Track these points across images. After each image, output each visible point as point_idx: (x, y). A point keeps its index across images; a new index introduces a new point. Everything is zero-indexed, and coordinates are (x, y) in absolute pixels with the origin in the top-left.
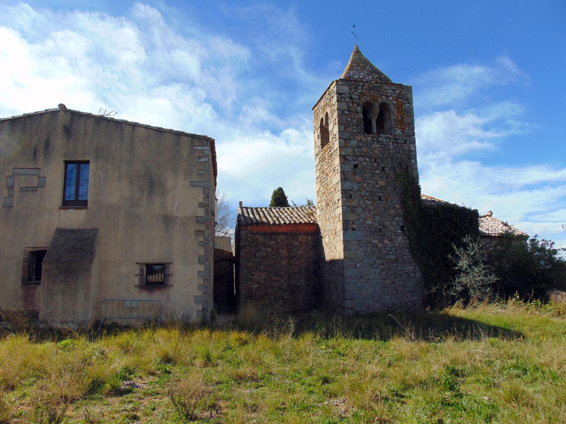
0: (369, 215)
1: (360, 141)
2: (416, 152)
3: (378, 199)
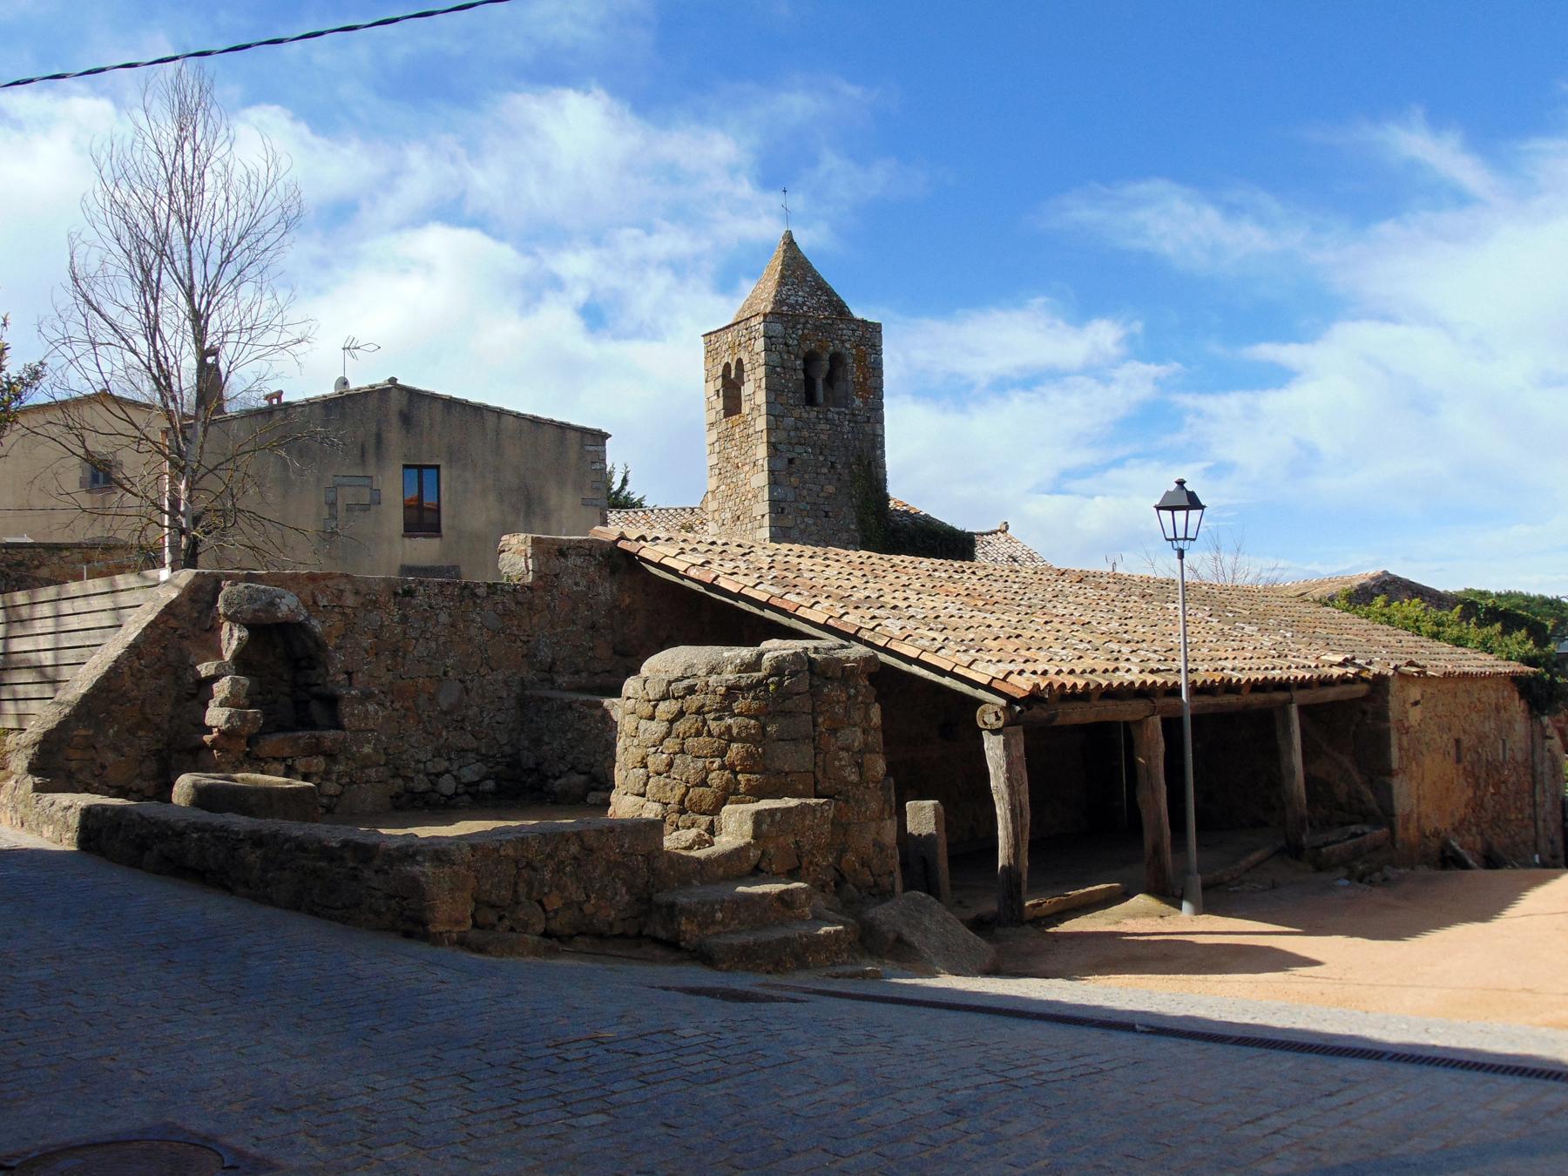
1: (799, 419)
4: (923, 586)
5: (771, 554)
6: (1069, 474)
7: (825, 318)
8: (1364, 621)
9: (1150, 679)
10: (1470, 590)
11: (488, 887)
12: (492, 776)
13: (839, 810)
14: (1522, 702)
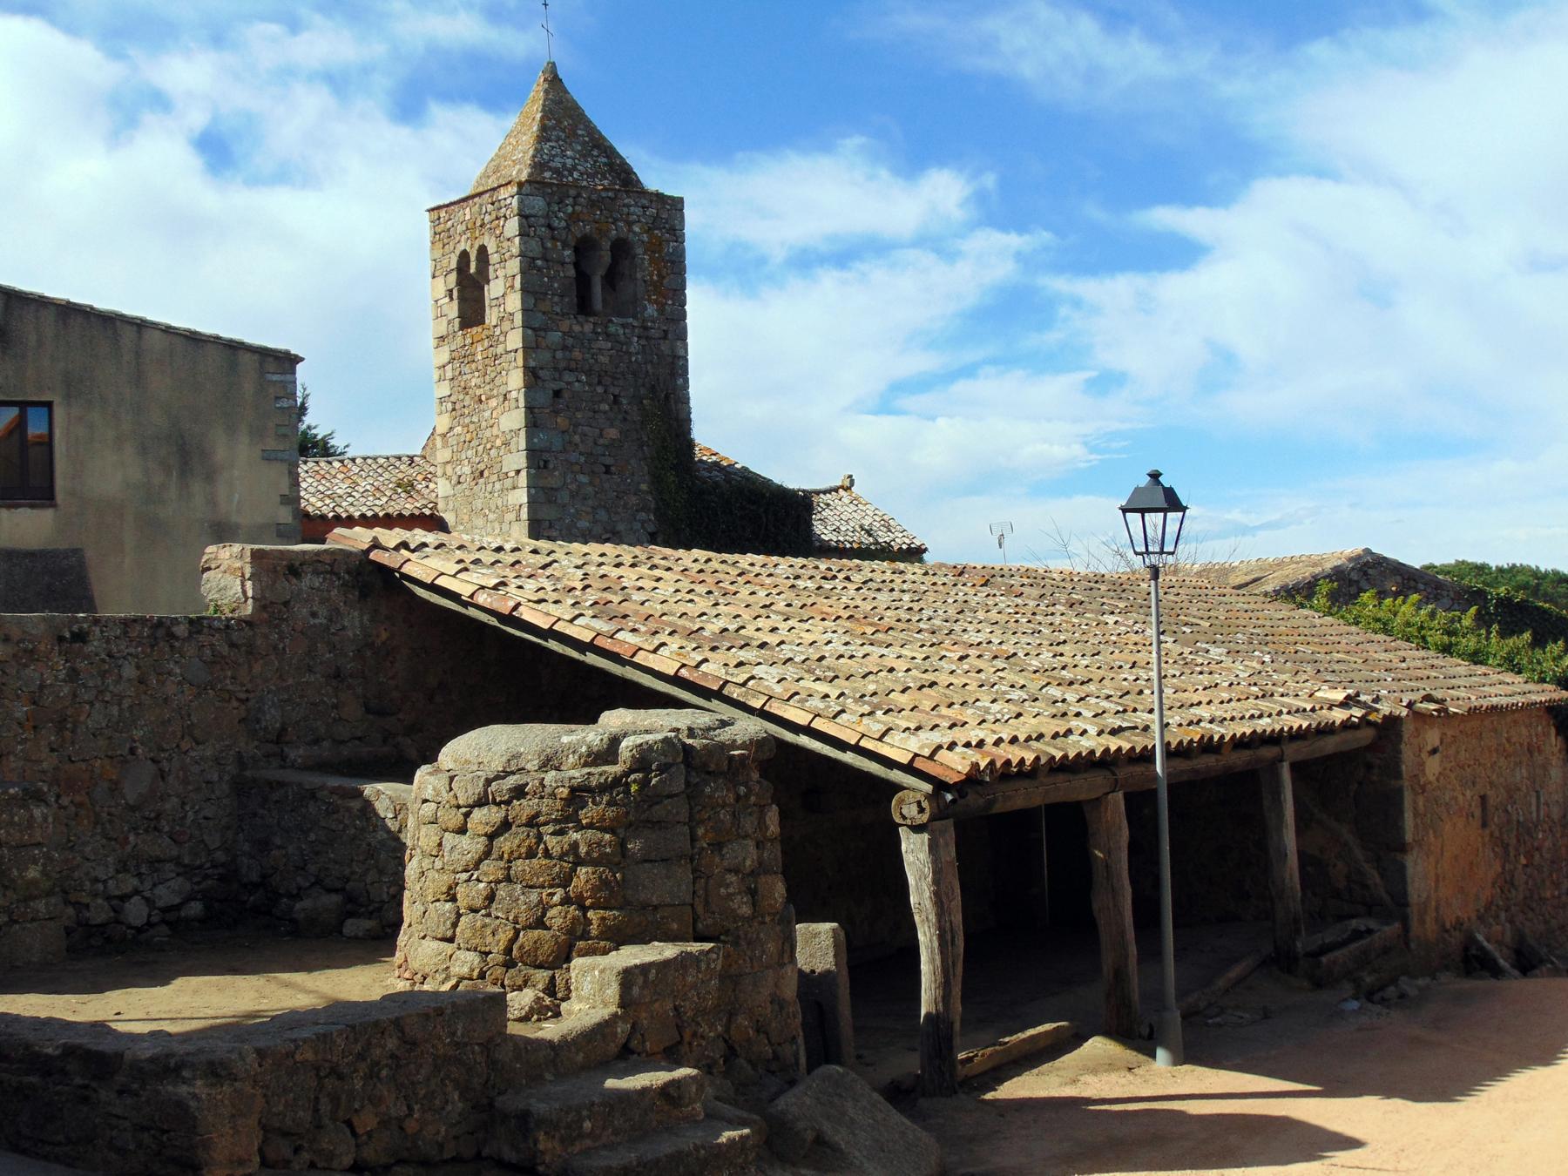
0: (584, 508)
1: (568, 333)
2: (687, 360)
3: (604, 469)
4: (789, 605)
5: (580, 562)
6: (901, 387)
7: (605, 189)
8: (1353, 629)
9: (1114, 743)
10: (1463, 562)
11: (281, 1108)
12: (199, 896)
13: (727, 956)
14: (1559, 738)
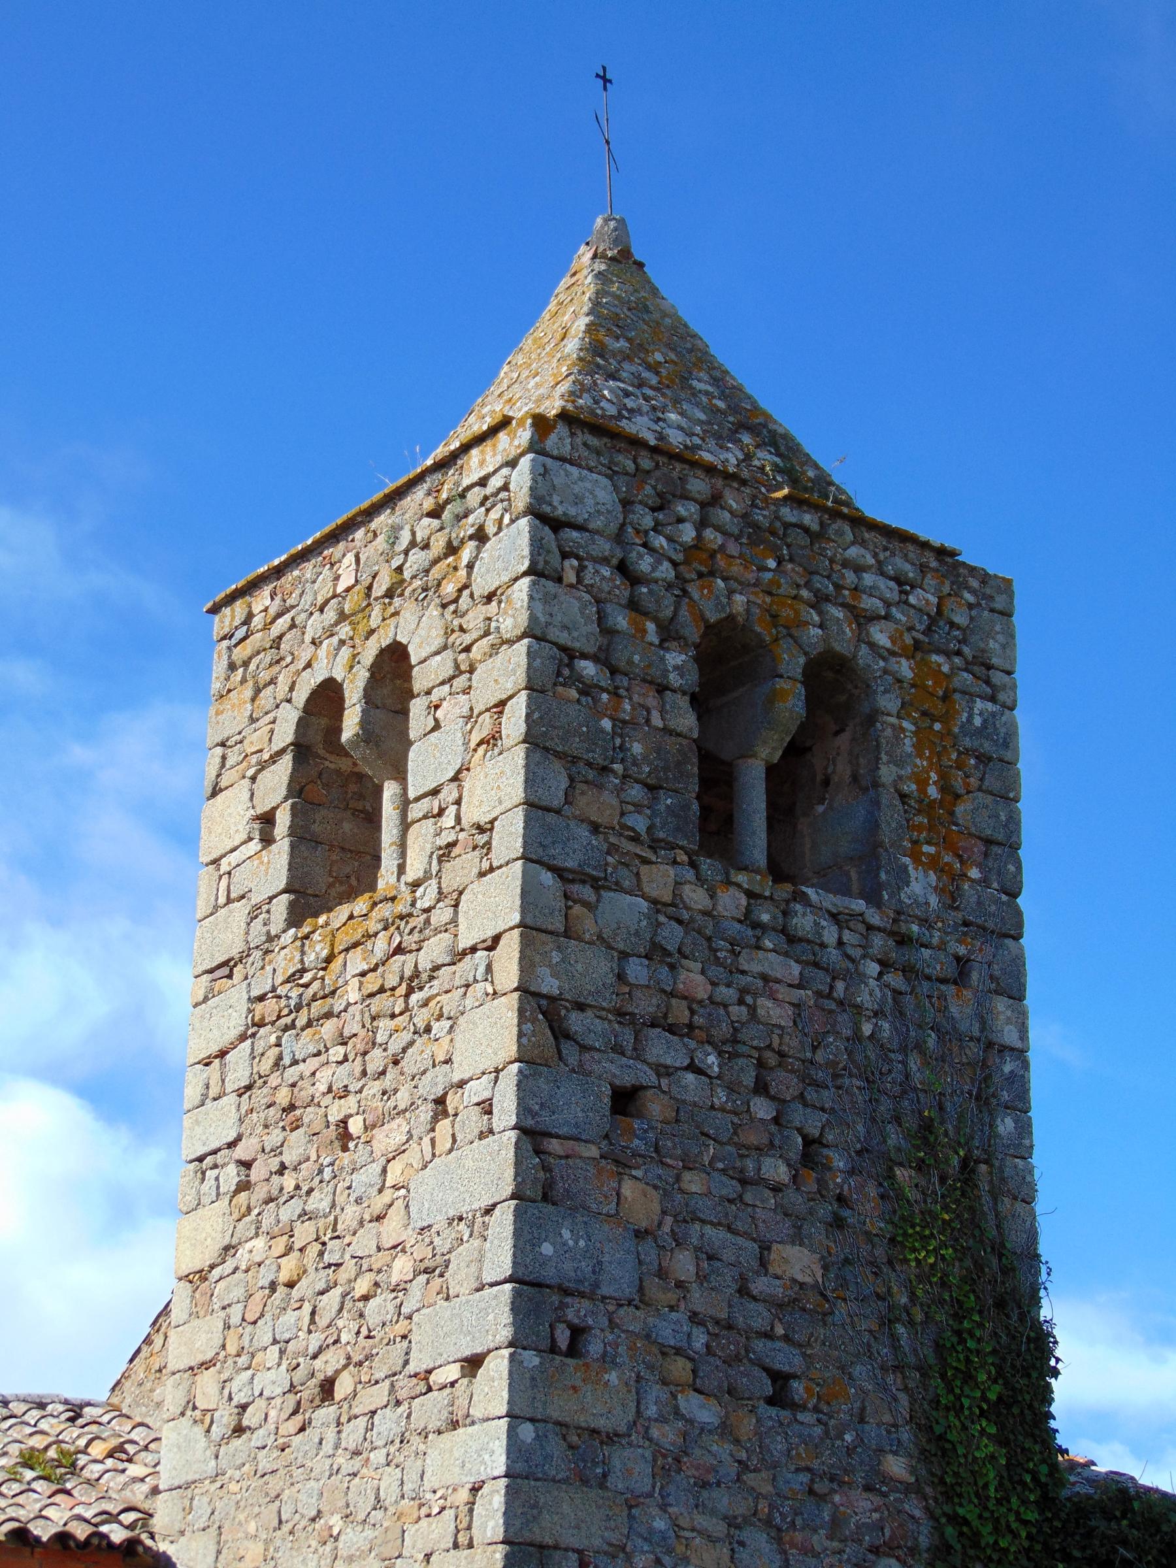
0: (701, 1521)
